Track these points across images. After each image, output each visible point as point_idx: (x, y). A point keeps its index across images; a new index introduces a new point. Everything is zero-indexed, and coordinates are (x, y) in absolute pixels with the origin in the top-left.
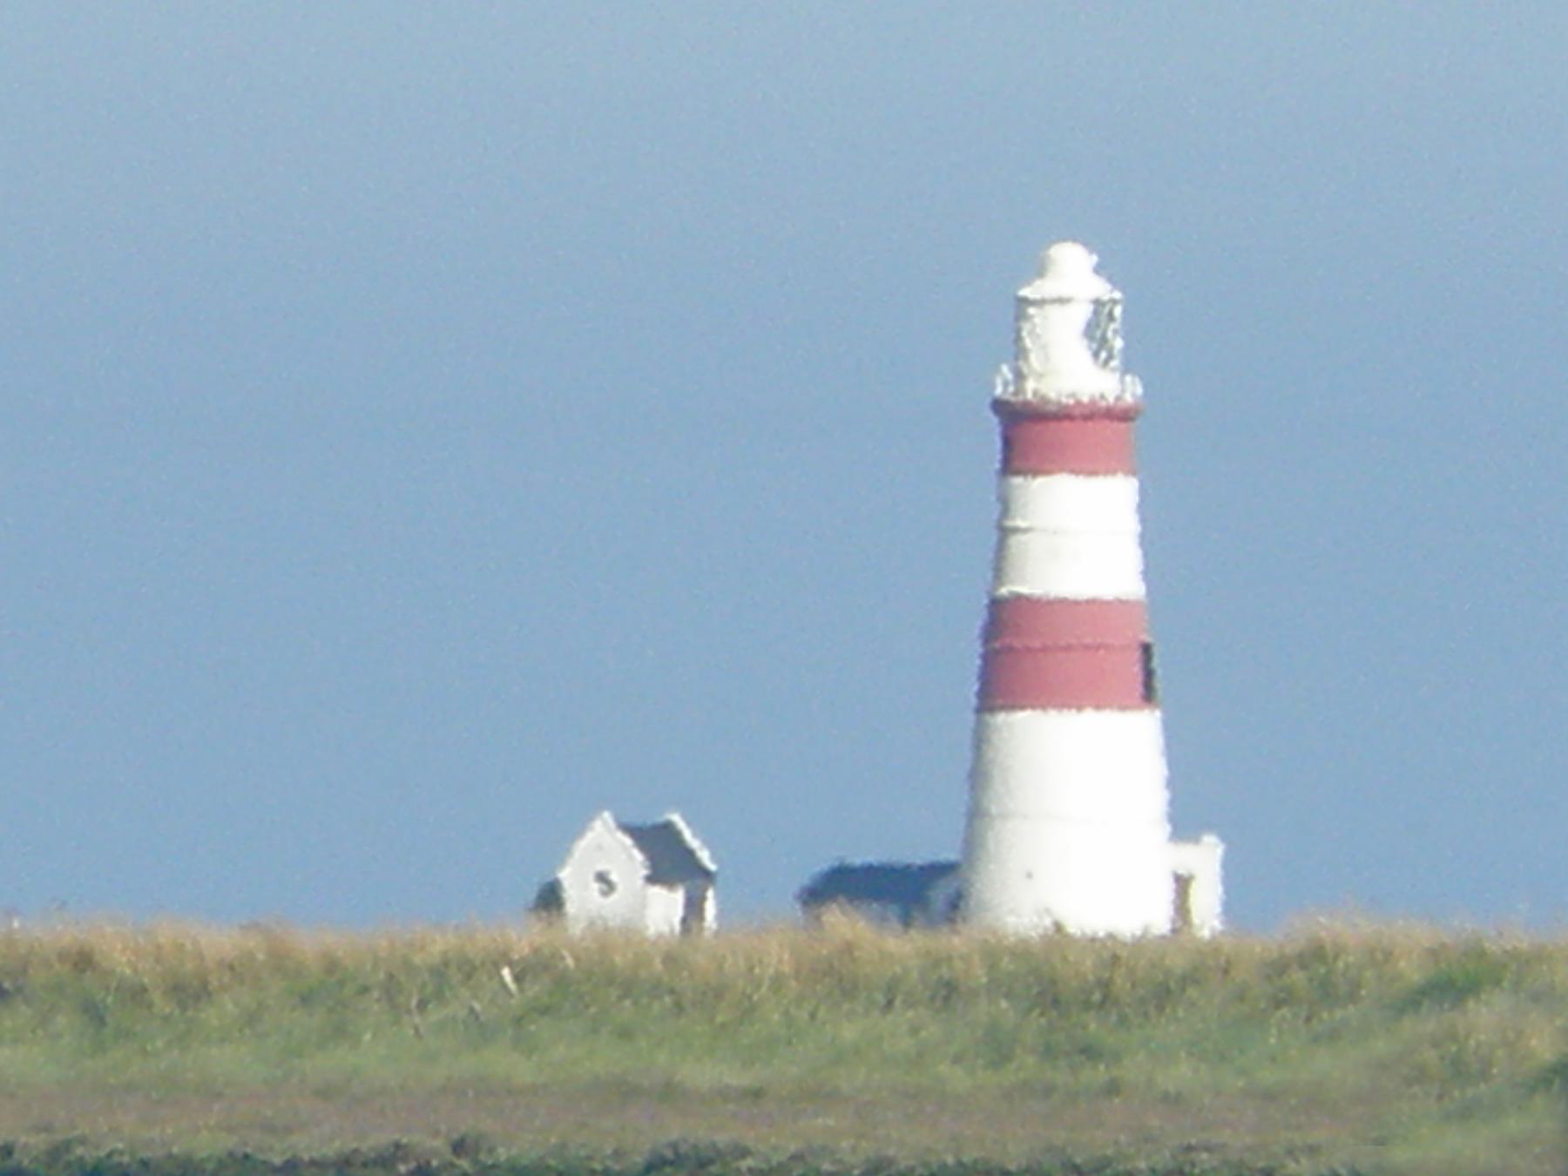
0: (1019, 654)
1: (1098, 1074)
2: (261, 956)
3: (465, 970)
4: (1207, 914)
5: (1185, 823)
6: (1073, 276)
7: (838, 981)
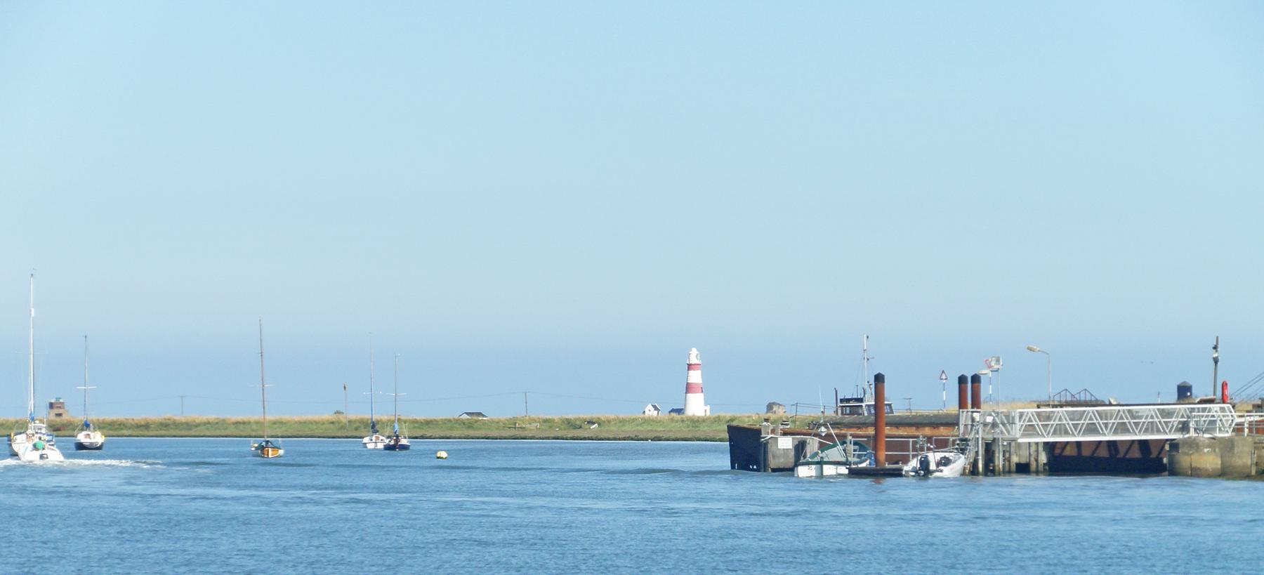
0: (689, 388)
3: (634, 420)
6: (694, 352)
7: (672, 420)
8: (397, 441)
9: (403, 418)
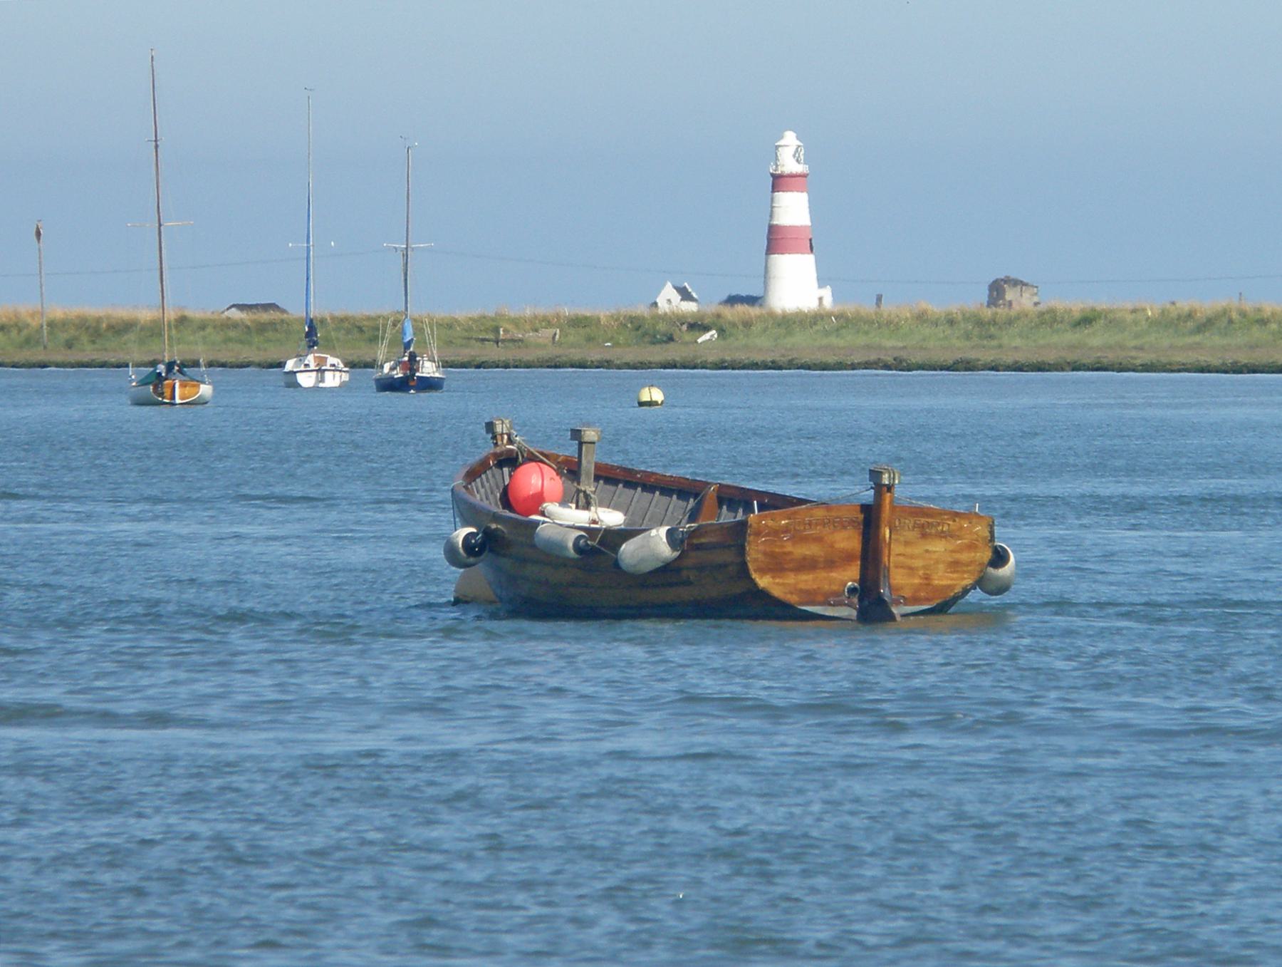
0: (776, 240)
1: (994, 343)
4: (828, 303)
5: (821, 285)
6: (790, 140)
8: (413, 363)
9: (195, 313)
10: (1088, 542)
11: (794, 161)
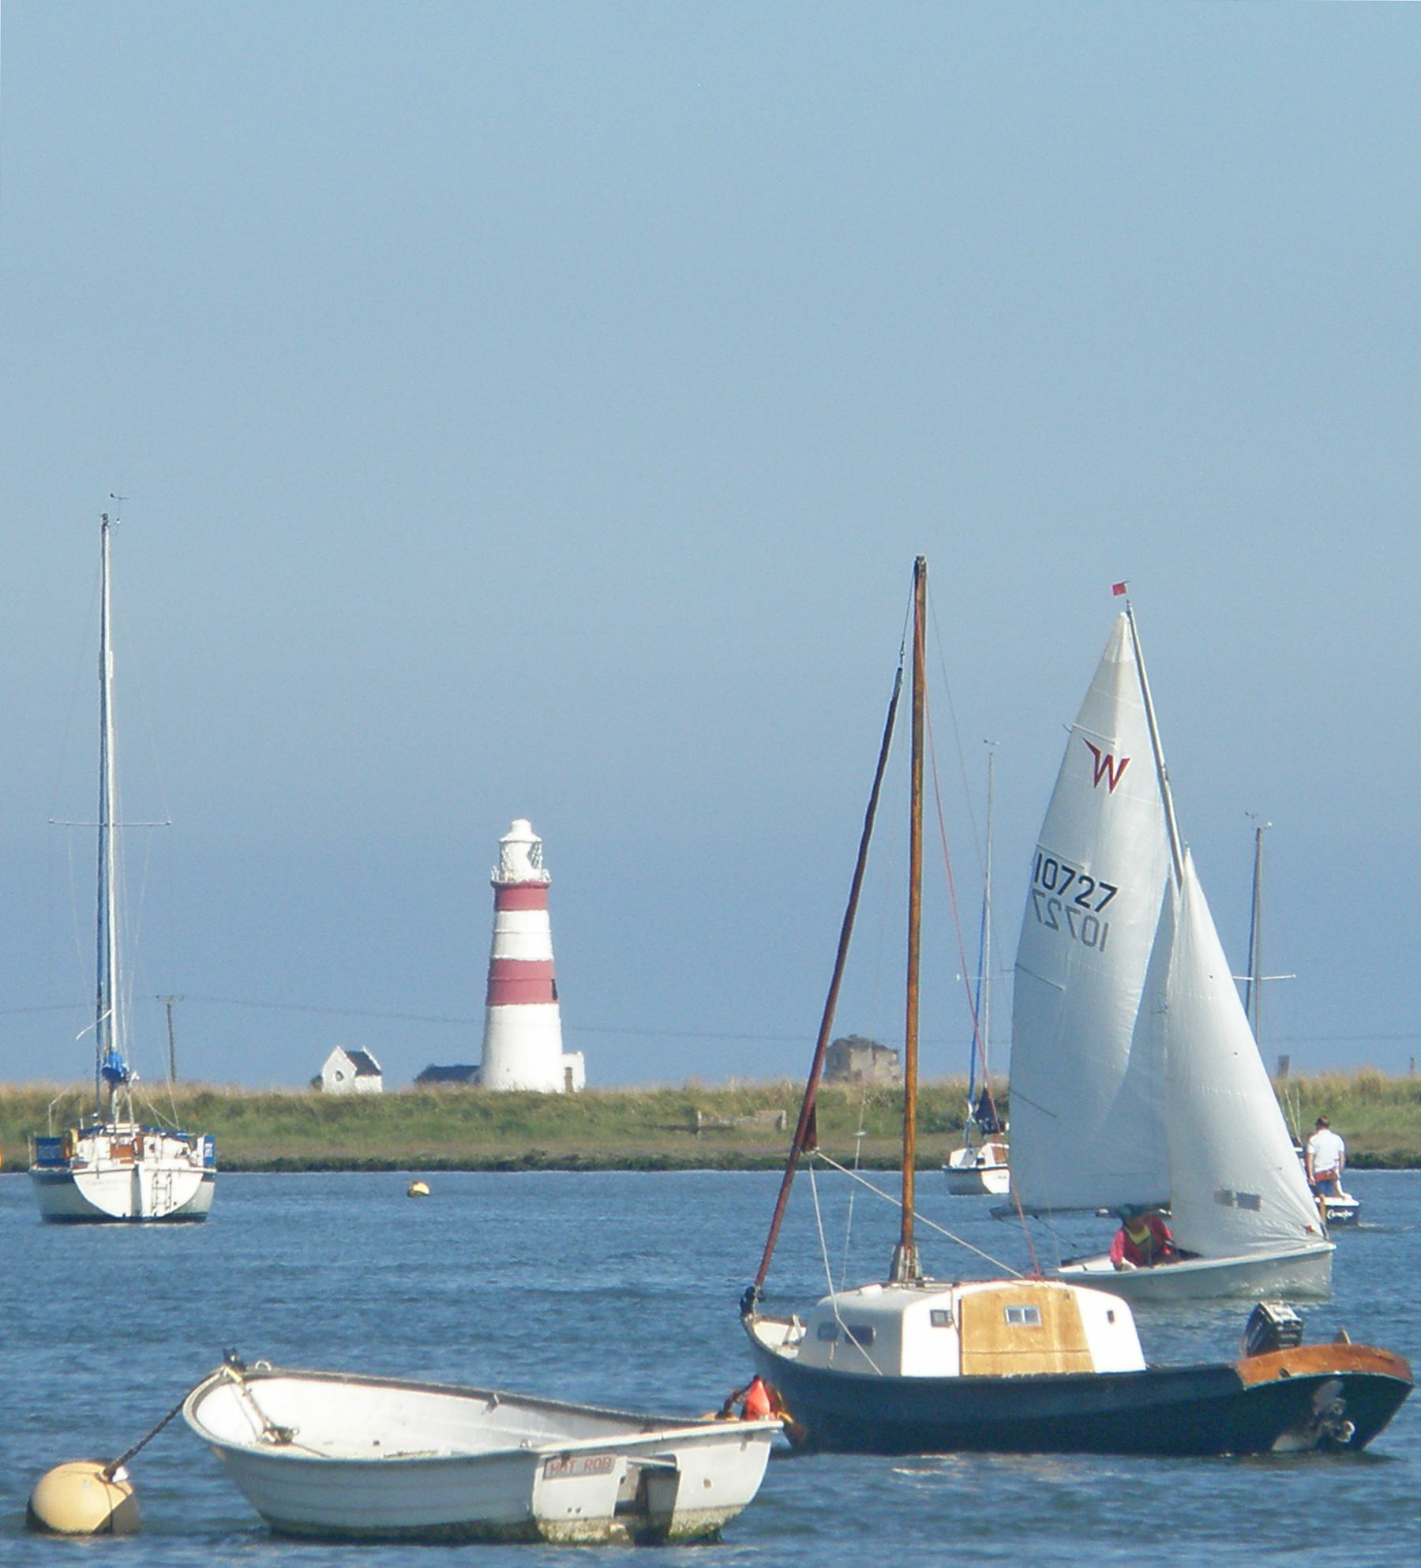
0: (503, 982)
2: (848, 1101)
4: (579, 1081)
5: (568, 1048)
6: (522, 831)
7: (425, 1101)
10: (15, 1454)
11: (528, 863)
